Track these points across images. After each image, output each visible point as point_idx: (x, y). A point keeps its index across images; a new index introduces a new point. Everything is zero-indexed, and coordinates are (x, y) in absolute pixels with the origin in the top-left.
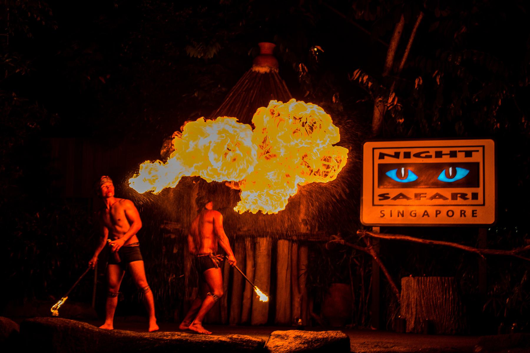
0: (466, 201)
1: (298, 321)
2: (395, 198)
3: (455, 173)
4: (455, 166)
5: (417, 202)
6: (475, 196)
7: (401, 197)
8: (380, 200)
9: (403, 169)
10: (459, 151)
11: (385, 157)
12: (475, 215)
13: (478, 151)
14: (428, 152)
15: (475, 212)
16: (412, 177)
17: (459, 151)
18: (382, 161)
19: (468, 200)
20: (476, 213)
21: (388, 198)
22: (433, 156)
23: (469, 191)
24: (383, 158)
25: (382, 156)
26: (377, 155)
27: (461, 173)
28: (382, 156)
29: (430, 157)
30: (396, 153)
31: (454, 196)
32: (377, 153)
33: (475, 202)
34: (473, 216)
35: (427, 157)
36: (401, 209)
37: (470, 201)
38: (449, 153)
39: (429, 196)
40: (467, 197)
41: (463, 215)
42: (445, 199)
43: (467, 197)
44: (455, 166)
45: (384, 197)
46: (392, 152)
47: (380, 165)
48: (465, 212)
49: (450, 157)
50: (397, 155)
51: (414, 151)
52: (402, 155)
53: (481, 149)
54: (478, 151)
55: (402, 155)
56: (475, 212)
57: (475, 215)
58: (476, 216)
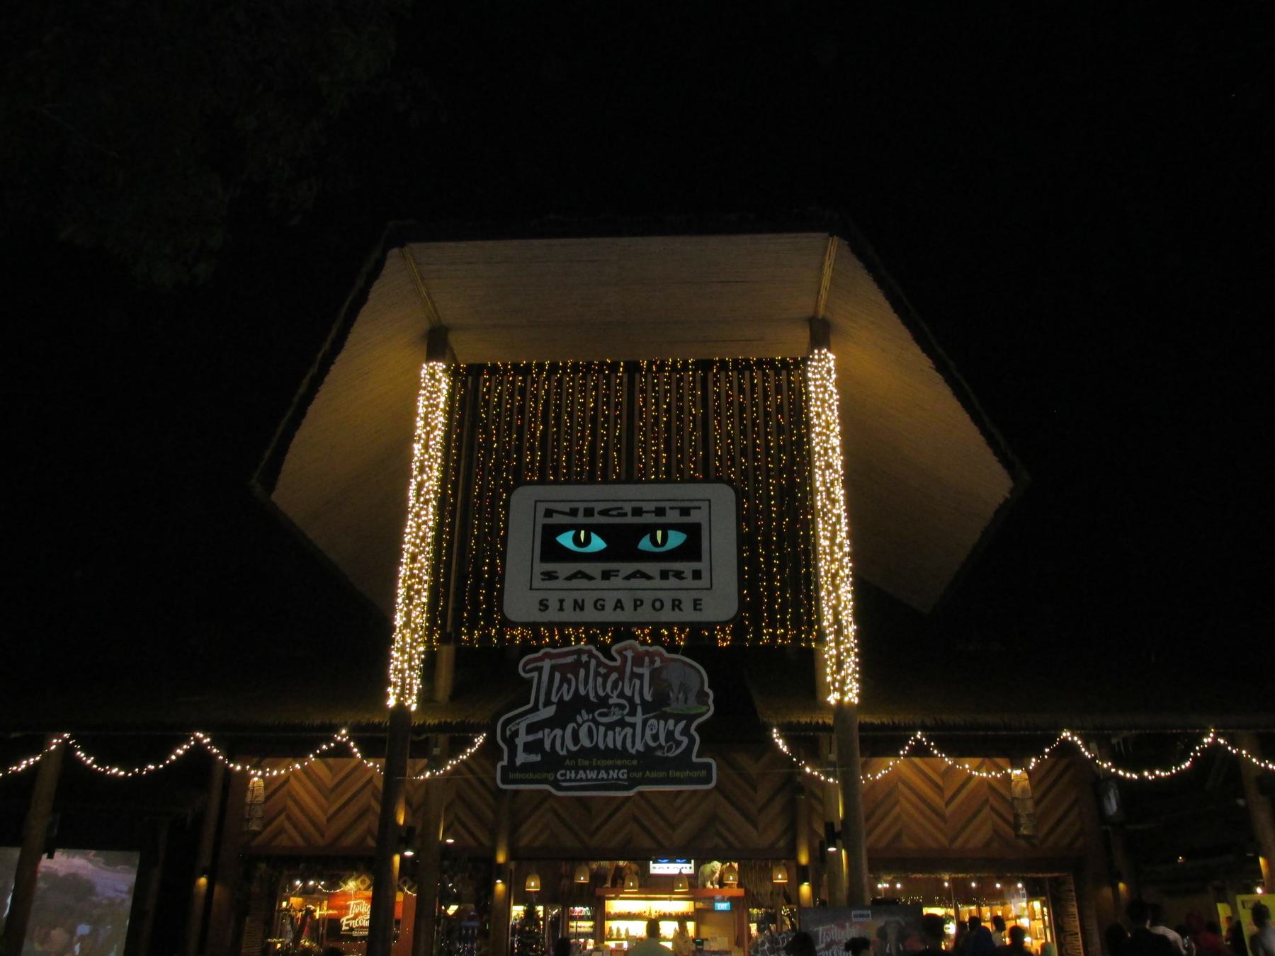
0: (592, 582)
1: (473, 915)
2: (569, 578)
3: (825, 538)
4: (665, 528)
5: (605, 584)
6: (697, 575)
7: (638, 575)
8: (543, 580)
9: (582, 533)
10: (671, 508)
11: (554, 515)
12: (698, 607)
13: (699, 508)
14: (621, 508)
15: (698, 602)
16: (598, 544)
17: (671, 508)
18: (549, 521)
19: (653, 581)
20: (700, 604)
21: (557, 578)
22: (543, 513)
23: (687, 567)
24: (551, 516)
25: (549, 513)
26: (541, 512)
27: (676, 539)
28: (549, 513)
29: (625, 515)
30: (572, 510)
31: (664, 575)
32: (542, 508)
33: (697, 584)
34: (695, 609)
35: (620, 515)
36: (578, 596)
37: (689, 582)
38: (654, 509)
39: (622, 575)
40: (683, 575)
41: (676, 609)
42: (590, 578)
43: (683, 575)
44: (665, 528)
45: (549, 576)
46: (566, 507)
47: (545, 527)
48: (680, 602)
49: (656, 515)
50: (574, 512)
51: (599, 507)
52: (581, 513)
53: (705, 505)
54: (699, 508)
55: (581, 513)
56: (698, 602)
57: (698, 607)
58: (700, 610)
